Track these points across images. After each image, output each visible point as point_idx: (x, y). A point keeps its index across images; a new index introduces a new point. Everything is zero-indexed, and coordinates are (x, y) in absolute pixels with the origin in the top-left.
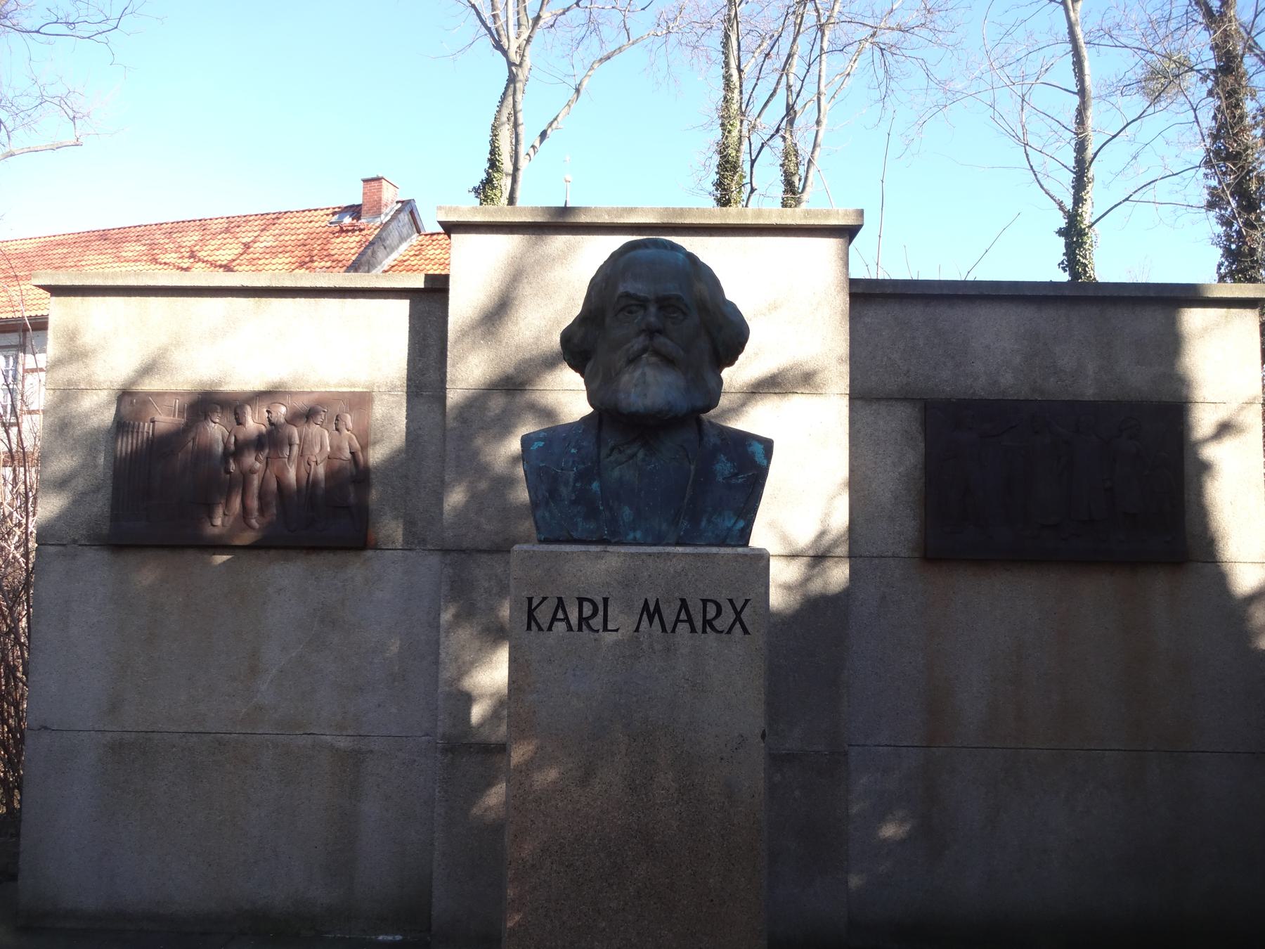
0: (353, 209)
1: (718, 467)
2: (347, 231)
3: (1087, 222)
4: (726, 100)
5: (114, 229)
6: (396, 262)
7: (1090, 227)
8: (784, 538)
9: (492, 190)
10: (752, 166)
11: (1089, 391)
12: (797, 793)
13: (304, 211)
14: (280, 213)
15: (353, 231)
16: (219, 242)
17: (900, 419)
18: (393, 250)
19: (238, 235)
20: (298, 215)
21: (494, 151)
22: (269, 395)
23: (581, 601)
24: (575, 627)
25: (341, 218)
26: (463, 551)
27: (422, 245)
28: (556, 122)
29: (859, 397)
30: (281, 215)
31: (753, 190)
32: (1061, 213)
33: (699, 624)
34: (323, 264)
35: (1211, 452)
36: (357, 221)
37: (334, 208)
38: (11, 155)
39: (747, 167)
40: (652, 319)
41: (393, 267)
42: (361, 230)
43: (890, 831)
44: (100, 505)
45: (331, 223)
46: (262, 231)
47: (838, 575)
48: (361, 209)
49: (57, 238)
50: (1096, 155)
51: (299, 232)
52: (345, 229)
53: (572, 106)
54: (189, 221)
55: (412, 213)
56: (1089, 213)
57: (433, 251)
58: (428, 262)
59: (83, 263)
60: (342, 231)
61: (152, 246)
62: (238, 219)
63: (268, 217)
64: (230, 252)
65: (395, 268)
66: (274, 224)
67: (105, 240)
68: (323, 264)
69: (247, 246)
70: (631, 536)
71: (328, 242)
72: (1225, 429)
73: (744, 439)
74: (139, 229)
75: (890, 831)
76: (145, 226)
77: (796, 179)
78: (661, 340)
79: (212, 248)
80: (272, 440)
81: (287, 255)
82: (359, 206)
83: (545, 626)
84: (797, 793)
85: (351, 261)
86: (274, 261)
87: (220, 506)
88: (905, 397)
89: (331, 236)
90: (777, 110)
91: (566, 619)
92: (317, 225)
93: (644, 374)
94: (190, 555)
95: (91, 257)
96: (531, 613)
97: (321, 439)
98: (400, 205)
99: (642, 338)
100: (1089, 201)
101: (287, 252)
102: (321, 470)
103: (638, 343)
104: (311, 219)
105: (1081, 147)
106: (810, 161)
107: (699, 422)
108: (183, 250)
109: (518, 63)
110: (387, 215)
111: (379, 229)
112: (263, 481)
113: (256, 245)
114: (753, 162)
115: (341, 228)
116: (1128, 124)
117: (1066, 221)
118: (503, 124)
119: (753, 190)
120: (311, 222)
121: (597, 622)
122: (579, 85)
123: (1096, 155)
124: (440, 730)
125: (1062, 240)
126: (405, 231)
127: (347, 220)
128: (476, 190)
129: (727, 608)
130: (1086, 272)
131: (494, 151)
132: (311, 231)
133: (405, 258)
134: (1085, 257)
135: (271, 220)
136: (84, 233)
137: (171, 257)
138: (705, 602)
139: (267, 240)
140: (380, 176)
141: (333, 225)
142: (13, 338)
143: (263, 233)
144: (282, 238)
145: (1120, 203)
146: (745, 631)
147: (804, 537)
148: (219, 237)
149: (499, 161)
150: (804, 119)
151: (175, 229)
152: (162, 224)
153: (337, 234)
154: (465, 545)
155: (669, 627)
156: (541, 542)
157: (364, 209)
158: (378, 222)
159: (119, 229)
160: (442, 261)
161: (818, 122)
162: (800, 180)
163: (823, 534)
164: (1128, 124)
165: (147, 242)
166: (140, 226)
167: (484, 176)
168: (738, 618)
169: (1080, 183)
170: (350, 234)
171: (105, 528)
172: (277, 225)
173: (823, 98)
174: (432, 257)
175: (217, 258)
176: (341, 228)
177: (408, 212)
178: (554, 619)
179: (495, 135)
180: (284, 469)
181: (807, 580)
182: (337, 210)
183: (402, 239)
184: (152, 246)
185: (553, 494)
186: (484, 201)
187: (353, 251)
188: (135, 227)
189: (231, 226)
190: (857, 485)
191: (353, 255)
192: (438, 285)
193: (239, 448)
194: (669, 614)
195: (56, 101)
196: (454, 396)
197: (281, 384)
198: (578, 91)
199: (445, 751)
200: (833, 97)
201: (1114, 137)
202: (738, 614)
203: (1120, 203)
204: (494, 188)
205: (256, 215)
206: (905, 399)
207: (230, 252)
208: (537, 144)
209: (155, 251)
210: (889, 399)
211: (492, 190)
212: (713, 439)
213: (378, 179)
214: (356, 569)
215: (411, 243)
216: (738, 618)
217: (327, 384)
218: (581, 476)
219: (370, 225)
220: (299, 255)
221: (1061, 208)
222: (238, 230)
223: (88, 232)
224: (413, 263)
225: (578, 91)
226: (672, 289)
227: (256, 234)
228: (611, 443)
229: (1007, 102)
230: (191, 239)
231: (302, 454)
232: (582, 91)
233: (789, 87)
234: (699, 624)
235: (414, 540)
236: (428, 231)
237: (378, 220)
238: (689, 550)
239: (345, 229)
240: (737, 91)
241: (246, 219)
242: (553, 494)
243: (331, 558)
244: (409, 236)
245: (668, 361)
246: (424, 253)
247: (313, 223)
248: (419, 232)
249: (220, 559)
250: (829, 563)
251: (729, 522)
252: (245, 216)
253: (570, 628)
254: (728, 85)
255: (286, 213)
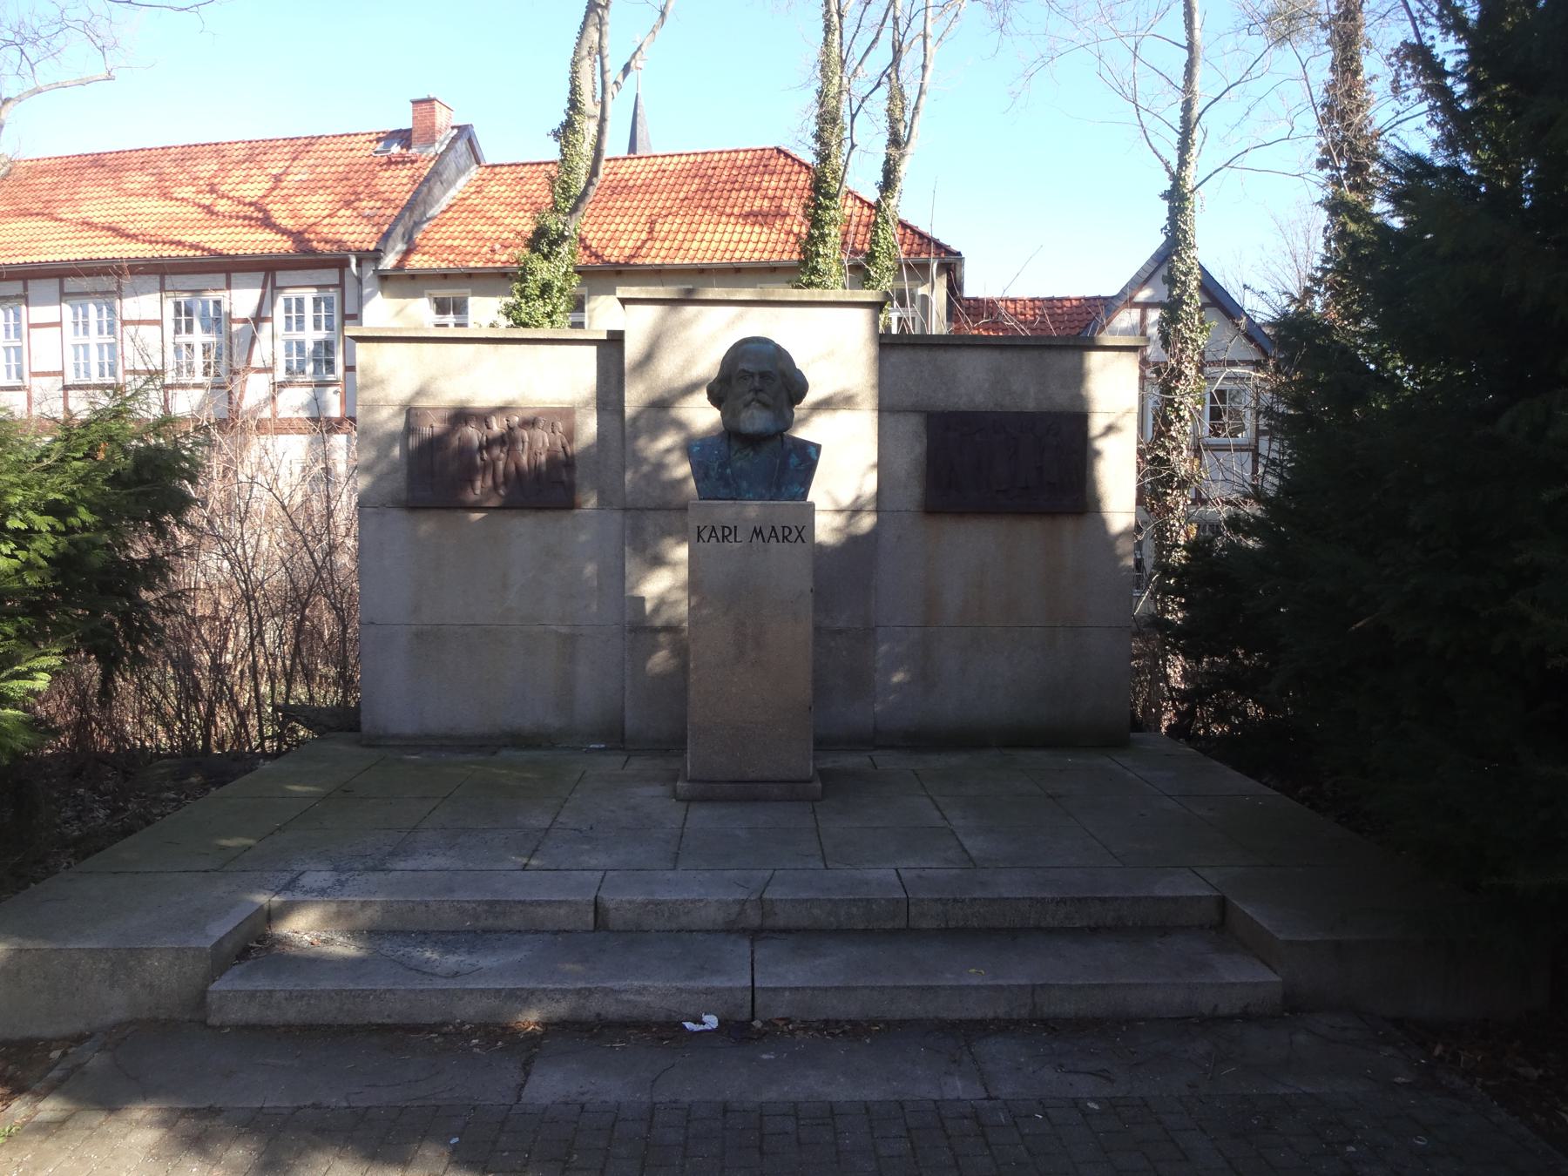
0: (400, 134)
1: (791, 460)
2: (397, 163)
3: (1189, 187)
4: (827, 43)
5: (111, 153)
6: (455, 201)
7: (1192, 192)
8: (835, 501)
9: (573, 134)
10: (852, 121)
11: (1030, 405)
12: (844, 653)
13: (342, 136)
14: (313, 138)
15: (404, 163)
16: (244, 173)
17: (912, 426)
18: (451, 184)
19: (266, 165)
20: (335, 140)
21: (575, 90)
22: (501, 410)
23: (723, 527)
24: (721, 539)
25: (388, 146)
26: (638, 509)
27: (484, 180)
28: (639, 53)
29: (886, 410)
30: (314, 141)
31: (853, 146)
32: (1167, 175)
33: (781, 538)
34: (372, 204)
35: (1100, 444)
36: (407, 150)
37: (378, 133)
38: (39, 92)
39: (848, 120)
40: (757, 384)
41: (452, 206)
42: (413, 162)
43: (898, 678)
44: (399, 481)
45: (376, 152)
46: (294, 160)
47: (867, 522)
48: (411, 135)
49: (42, 163)
50: (1200, 115)
51: (338, 162)
52: (393, 160)
53: (658, 33)
54: (203, 145)
55: (470, 141)
56: (1192, 176)
57: (495, 189)
58: (492, 201)
59: (81, 196)
60: (390, 162)
61: (161, 177)
62: (263, 145)
63: (299, 142)
64: (259, 186)
65: (455, 208)
66: (308, 152)
67: (103, 166)
68: (372, 204)
69: (278, 179)
70: (747, 496)
71: (375, 177)
72: (1110, 429)
73: (805, 445)
74: (142, 153)
75: (898, 678)
76: (150, 150)
77: (901, 126)
78: (762, 396)
79: (237, 180)
80: (507, 440)
81: (328, 191)
82: (409, 131)
83: (706, 540)
84: (844, 653)
85: (405, 201)
86: (314, 199)
87: (682, 567)
88: (915, 410)
89: (378, 168)
90: (883, 54)
91: (716, 536)
92: (360, 154)
93: (752, 413)
94: (460, 514)
95: (87, 191)
96: (699, 533)
97: (543, 440)
98: (455, 131)
99: (751, 393)
100: (1193, 165)
101: (328, 188)
102: (543, 458)
103: (749, 396)
104: (352, 146)
105: (1187, 107)
106: (916, 108)
107: (782, 435)
108: (201, 182)
109: (603, 4)
110: (441, 144)
111: (434, 162)
112: (506, 465)
113: (289, 178)
114: (853, 117)
115: (389, 158)
116: (1229, 88)
117: (1171, 183)
118: (583, 59)
119: (853, 146)
120: (351, 150)
121: (731, 538)
122: (665, 6)
123: (1200, 115)
124: (627, 619)
125: (1166, 204)
126: (462, 162)
127: (396, 149)
128: (556, 134)
129: (794, 530)
130: (1186, 239)
131: (575, 90)
132: (354, 161)
133: (464, 196)
134: (1185, 223)
135: (302, 147)
136: (74, 156)
137: (187, 192)
138: (784, 527)
139: (299, 174)
140: (432, 96)
141: (379, 155)
142: (16, 287)
143: (295, 164)
144: (318, 170)
145: (1210, 176)
146: (803, 541)
147: (846, 500)
148: (244, 166)
149: (580, 102)
150: (910, 60)
151: (187, 154)
152: (169, 148)
153: (385, 167)
154: (639, 506)
155: (766, 540)
156: (700, 499)
157: (415, 135)
158: (432, 152)
159: (118, 153)
160: (509, 200)
161: (924, 67)
162: (906, 127)
163: (858, 497)
164: (1229, 88)
165: (155, 171)
166: (143, 150)
167: (564, 118)
168: (800, 535)
169: (1184, 146)
170: (400, 166)
171: (403, 496)
172: (311, 153)
173: (928, 41)
174: (497, 195)
175: (245, 194)
176: (389, 158)
177: (465, 140)
178: (710, 536)
179: (576, 72)
180: (519, 458)
181: (848, 525)
182: (381, 135)
183: (461, 172)
184: (161, 177)
185: (707, 476)
186: (565, 146)
187: (406, 188)
188: (137, 151)
189: (255, 152)
190: (882, 466)
191: (407, 192)
192: (616, 338)
193: (489, 445)
194: (766, 533)
195: (80, 25)
196: (629, 411)
197: (514, 402)
198: (663, 14)
199: (631, 631)
200: (940, 39)
201: (1216, 99)
202: (800, 533)
203: (1210, 176)
204: (575, 132)
205: (285, 139)
206: (915, 411)
207: (259, 186)
208: (620, 79)
209: (167, 184)
210: (905, 411)
211: (573, 134)
212: (789, 446)
213: (430, 101)
214: (566, 520)
215: (469, 178)
216: (800, 535)
217: (545, 402)
218: (720, 466)
219: (425, 155)
220: (343, 191)
221: (1168, 169)
222: (265, 158)
223: (79, 156)
224: (476, 202)
225: (663, 14)
226: (767, 367)
227: (287, 164)
228: (736, 448)
229: (1118, 54)
230: (206, 169)
231: (530, 448)
232: (668, 14)
233: (896, 20)
234: (781, 538)
235: (603, 503)
236: (488, 163)
237: (431, 149)
238: (776, 502)
239: (393, 160)
240: (837, 33)
241: (271, 145)
242: (707, 476)
243: (550, 514)
244: (467, 168)
245: (765, 406)
246: (486, 190)
247: (355, 152)
248: (478, 162)
249: (477, 516)
250: (863, 514)
251: (796, 489)
252: (271, 140)
253: (718, 540)
254: (828, 29)
255: (320, 137)
